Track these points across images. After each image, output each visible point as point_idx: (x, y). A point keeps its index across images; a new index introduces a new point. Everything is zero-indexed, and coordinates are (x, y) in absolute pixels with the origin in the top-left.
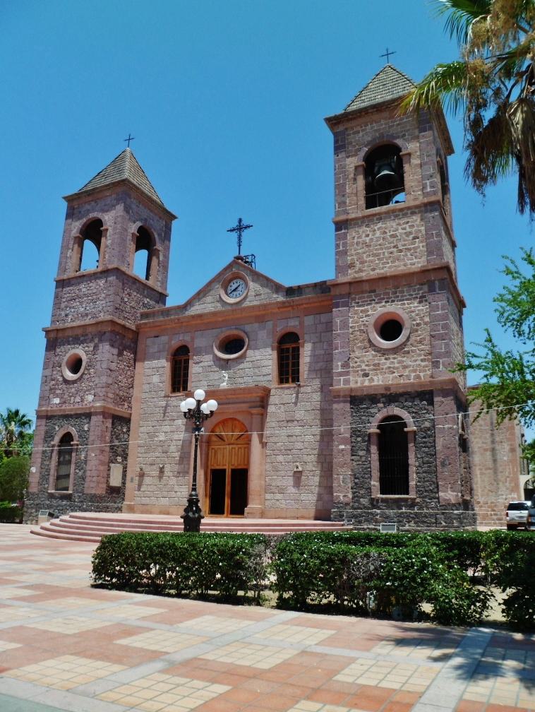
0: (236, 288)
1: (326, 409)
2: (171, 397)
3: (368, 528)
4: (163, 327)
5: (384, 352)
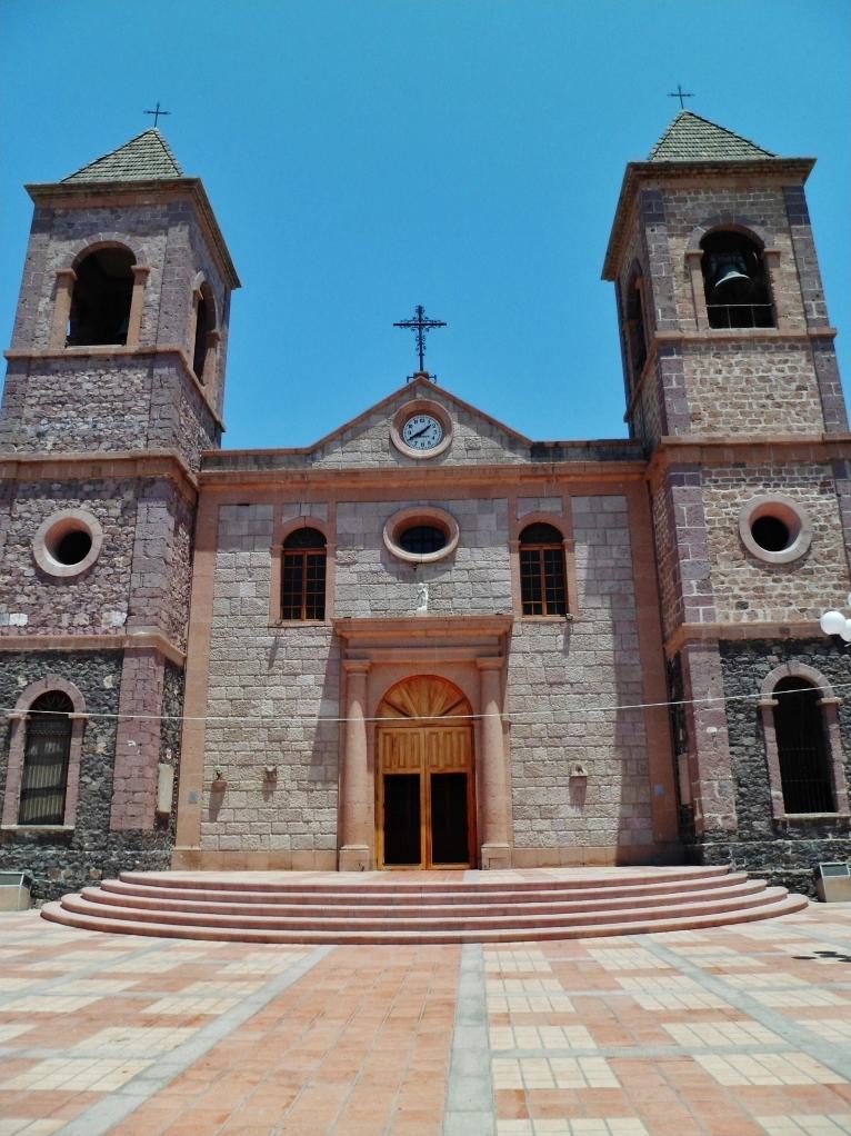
0: (423, 432)
1: (625, 665)
2: (286, 628)
3: (776, 874)
4: (262, 487)
5: (771, 569)
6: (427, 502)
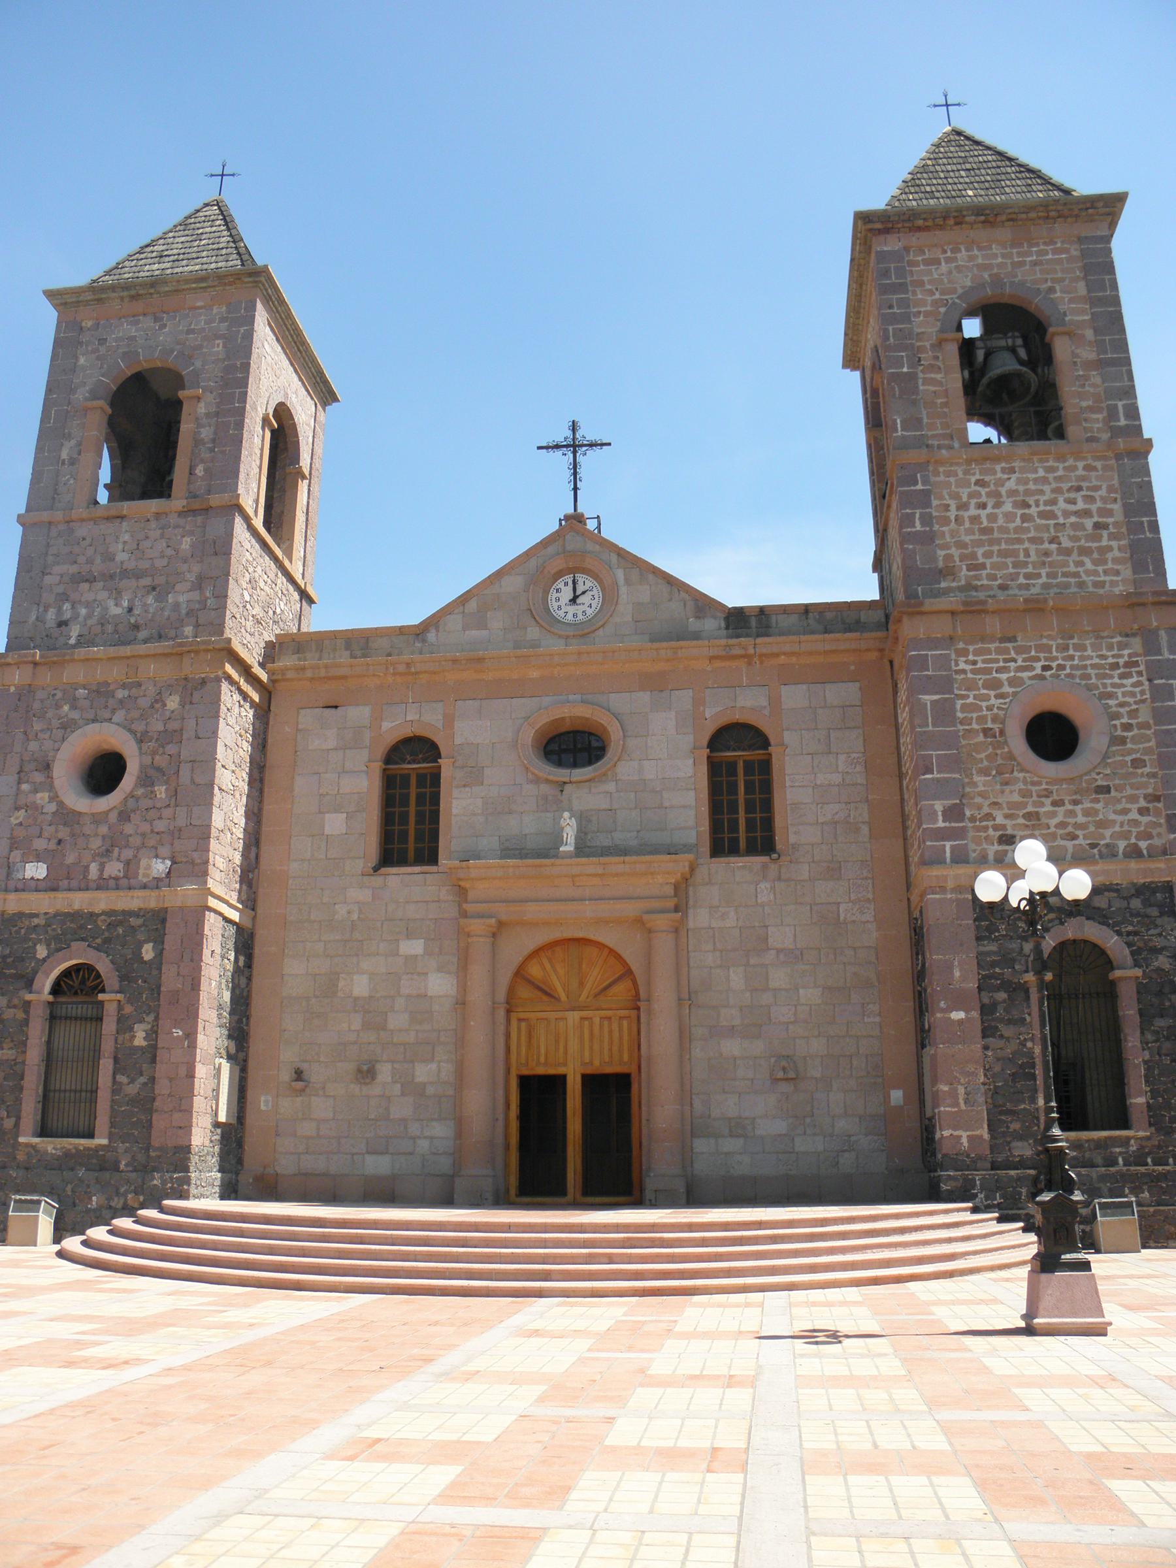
6: (578, 697)
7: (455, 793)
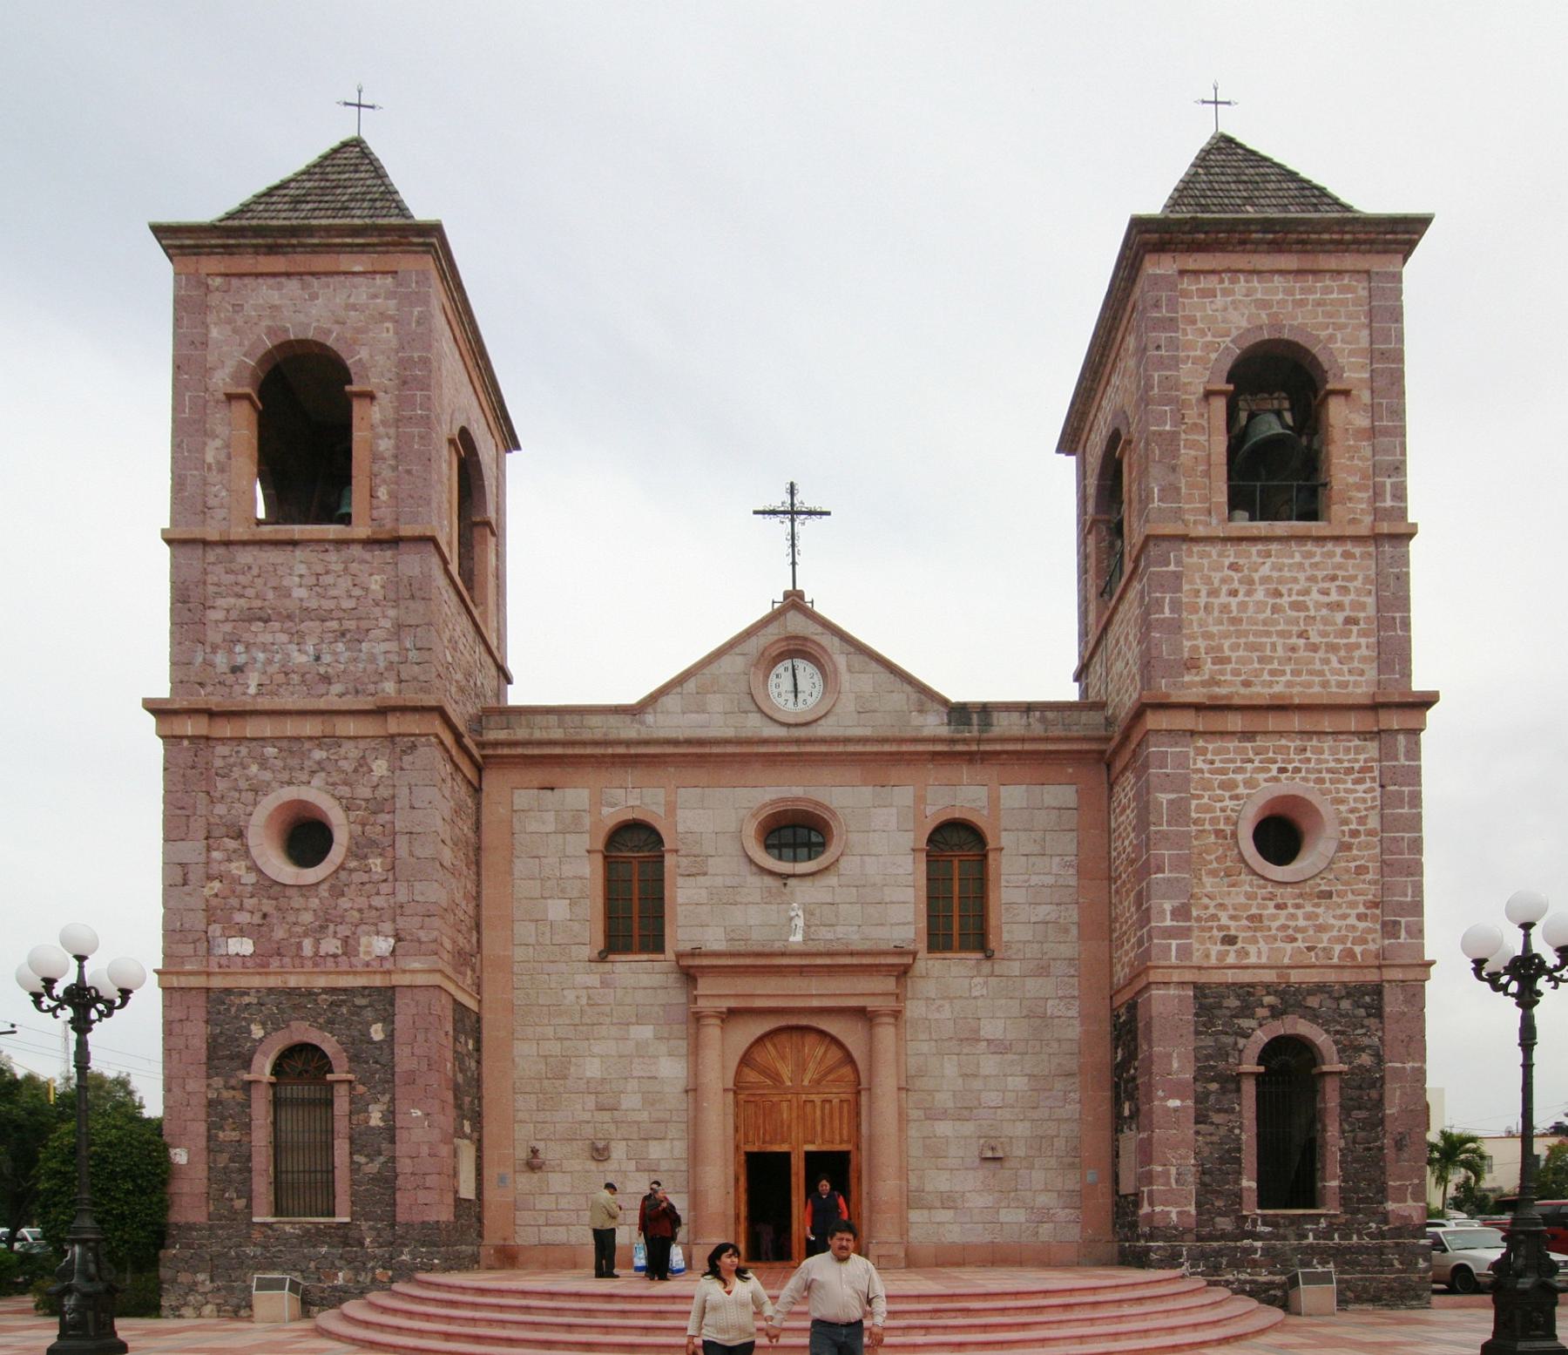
7: (680, 881)
